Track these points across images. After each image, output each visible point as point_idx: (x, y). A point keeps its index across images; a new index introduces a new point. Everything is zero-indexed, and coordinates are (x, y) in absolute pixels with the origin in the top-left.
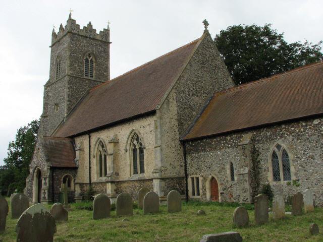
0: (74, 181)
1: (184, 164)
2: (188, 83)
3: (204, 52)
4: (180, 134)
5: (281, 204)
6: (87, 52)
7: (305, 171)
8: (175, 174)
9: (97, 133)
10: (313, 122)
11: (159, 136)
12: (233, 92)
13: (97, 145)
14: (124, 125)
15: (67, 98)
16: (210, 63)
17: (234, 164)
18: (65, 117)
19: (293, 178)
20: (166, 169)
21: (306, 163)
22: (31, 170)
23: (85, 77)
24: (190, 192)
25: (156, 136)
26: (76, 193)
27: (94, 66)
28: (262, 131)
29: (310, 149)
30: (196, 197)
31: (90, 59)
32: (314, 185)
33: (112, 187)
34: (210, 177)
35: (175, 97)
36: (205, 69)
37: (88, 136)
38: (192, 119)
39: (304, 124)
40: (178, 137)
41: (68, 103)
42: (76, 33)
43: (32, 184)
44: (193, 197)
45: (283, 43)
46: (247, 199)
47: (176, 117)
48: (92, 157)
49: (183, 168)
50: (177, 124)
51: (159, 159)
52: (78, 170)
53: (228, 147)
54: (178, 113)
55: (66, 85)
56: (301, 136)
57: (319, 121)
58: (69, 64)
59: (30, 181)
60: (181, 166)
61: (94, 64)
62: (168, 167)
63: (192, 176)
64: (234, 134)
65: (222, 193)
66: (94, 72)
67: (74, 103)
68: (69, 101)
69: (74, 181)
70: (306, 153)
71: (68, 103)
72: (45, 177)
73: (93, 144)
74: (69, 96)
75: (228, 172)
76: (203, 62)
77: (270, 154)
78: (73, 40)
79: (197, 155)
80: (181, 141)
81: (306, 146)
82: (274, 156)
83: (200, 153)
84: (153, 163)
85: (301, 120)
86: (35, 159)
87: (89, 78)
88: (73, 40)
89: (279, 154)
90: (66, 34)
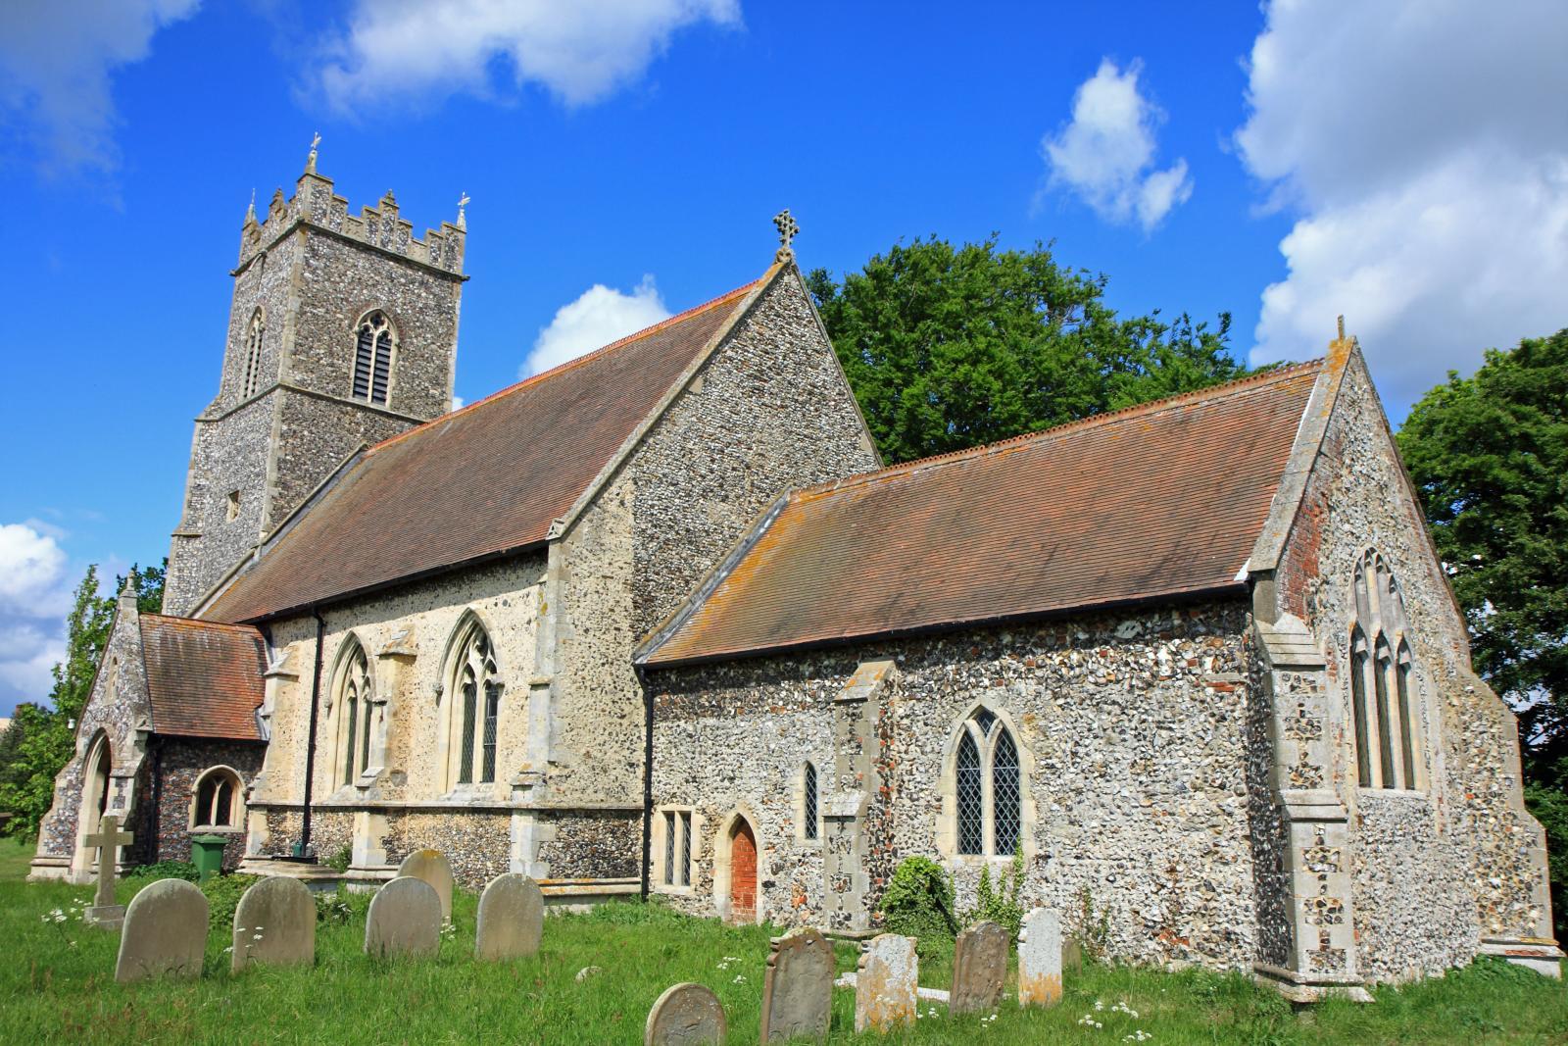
0: (247, 796)
1: (643, 759)
2: (690, 445)
3: (767, 334)
4: (637, 639)
5: (896, 972)
6: (367, 304)
7: (1072, 823)
8: (601, 795)
9: (348, 612)
10: (1114, 630)
11: (550, 643)
12: (873, 486)
13: (458, 642)
14: (440, 591)
15: (272, 475)
16: (790, 377)
17: (817, 769)
18: (259, 543)
19: (1029, 847)
20: (566, 772)
21: (1079, 792)
22: (81, 743)
23: (351, 399)
24: (657, 872)
25: (540, 640)
26: (250, 840)
27: (392, 361)
28: (930, 653)
29: (1096, 737)
30: (678, 888)
31: (377, 333)
32: (1103, 882)
33: (371, 829)
34: (731, 817)
35: (629, 499)
36: (766, 399)
37: (316, 622)
38: (694, 585)
39: (1082, 636)
40: (627, 650)
41: (276, 491)
42: (332, 228)
43: (79, 799)
44: (666, 889)
45: (1096, 317)
46: (848, 918)
47: (628, 572)
48: (322, 710)
49: (641, 771)
50: (628, 599)
51: (542, 730)
52: (269, 752)
53: (804, 706)
54: (639, 560)
55: (273, 424)
56: (1069, 682)
57: (1139, 629)
58: (291, 346)
59: (70, 786)
60: (632, 765)
61: (393, 352)
62: (574, 765)
63: (669, 807)
64: (829, 657)
65: (768, 885)
66: (391, 382)
67: (299, 495)
68: (281, 483)
69: (247, 796)
70: (1081, 751)
71: (276, 491)
72: (121, 773)
73: (328, 658)
74: (281, 464)
75: (799, 802)
76: (761, 372)
77: (951, 742)
78: (315, 253)
79: (690, 729)
80: (637, 668)
81: (1081, 724)
82: (967, 750)
83: (703, 721)
84: (525, 737)
85: (1073, 621)
86: (98, 704)
87: (368, 402)
88: (315, 253)
89: (986, 746)
90: (291, 232)
